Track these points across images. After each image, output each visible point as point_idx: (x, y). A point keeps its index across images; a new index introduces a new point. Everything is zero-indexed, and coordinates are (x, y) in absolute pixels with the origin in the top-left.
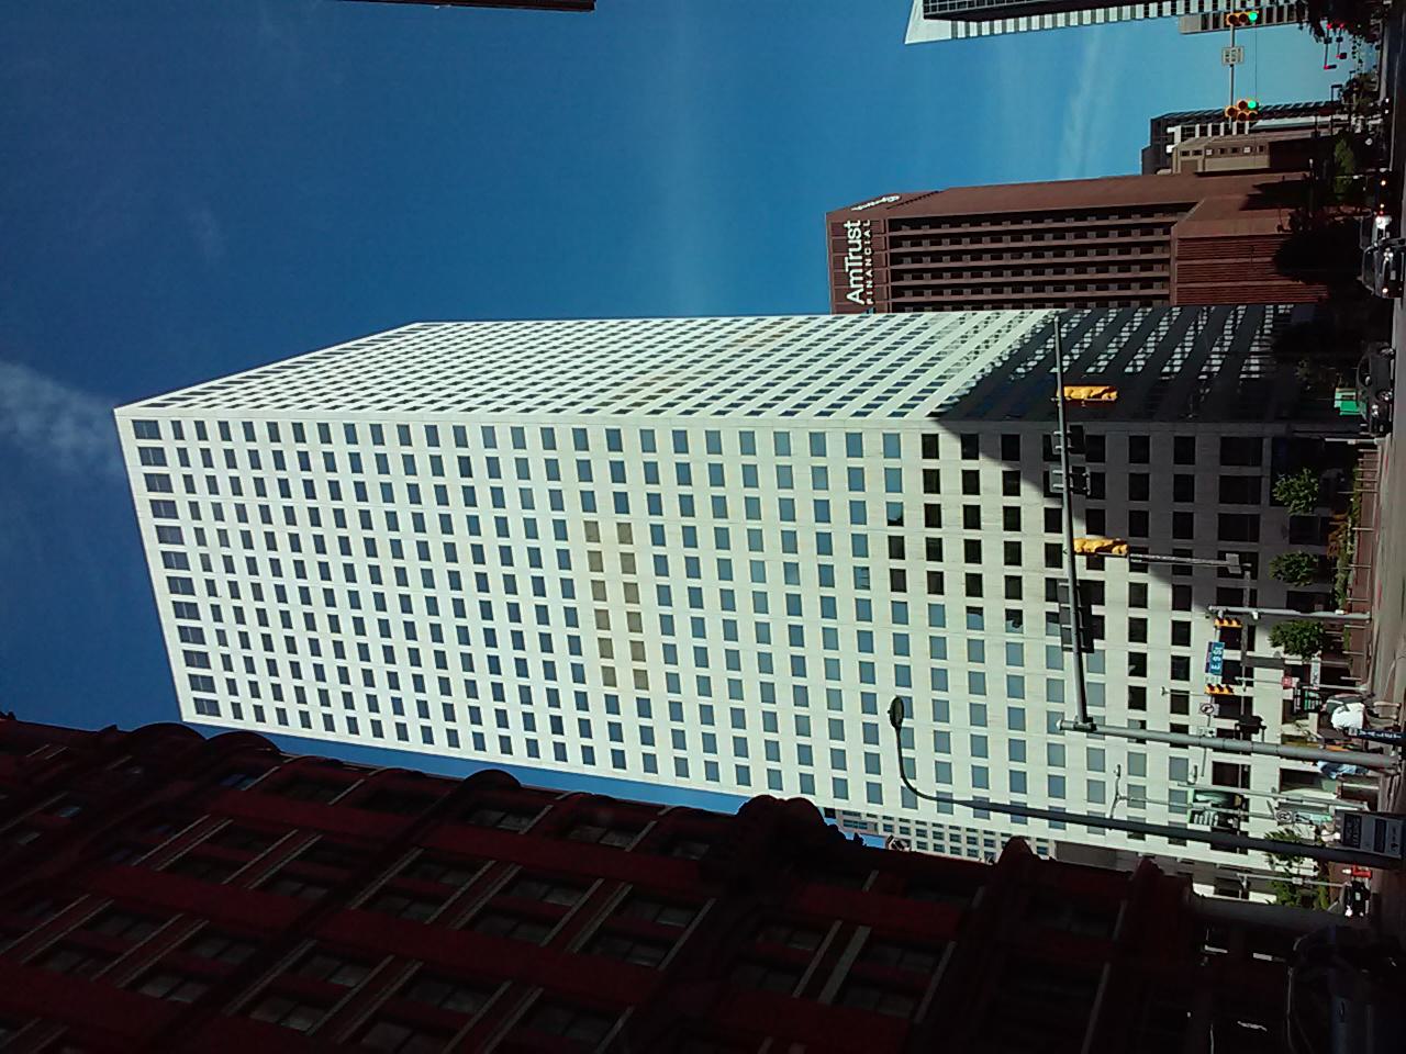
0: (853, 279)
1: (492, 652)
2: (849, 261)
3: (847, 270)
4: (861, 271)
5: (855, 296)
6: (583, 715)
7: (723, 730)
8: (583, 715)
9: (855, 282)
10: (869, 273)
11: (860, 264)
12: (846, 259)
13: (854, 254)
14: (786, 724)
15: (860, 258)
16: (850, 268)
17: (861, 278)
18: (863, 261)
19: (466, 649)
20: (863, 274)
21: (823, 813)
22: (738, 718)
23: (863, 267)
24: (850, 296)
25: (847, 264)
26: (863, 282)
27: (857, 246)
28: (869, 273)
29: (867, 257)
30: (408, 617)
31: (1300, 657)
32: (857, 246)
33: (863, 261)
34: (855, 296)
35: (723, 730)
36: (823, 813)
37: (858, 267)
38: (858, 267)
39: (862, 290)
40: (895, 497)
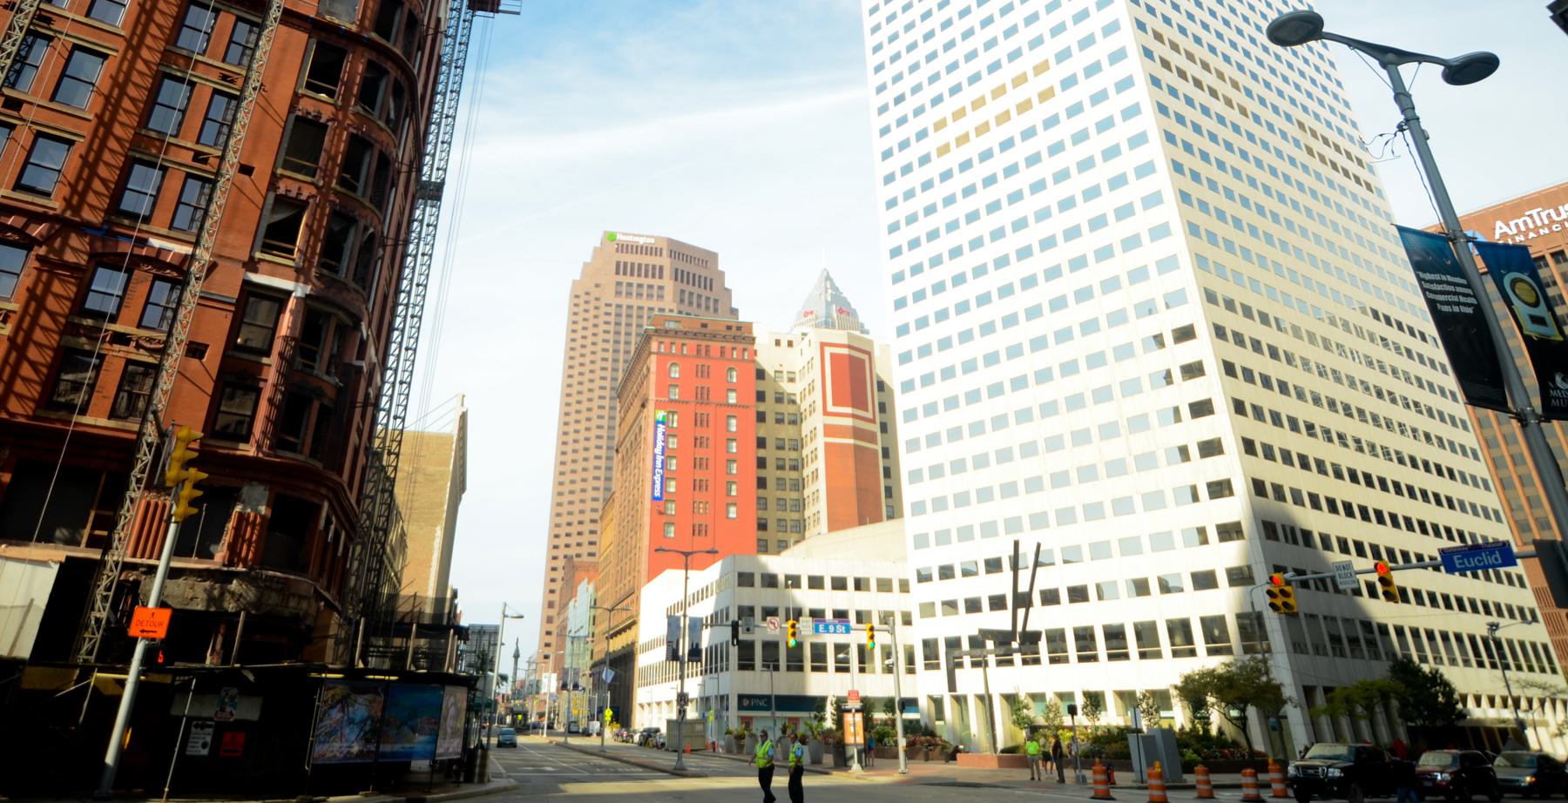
0: (1520, 221)
1: (1118, 119)
2: (1539, 213)
3: (1527, 213)
4: (1531, 226)
5: (1501, 228)
6: (1050, 181)
7: (1108, 202)
8: (1050, 181)
9: (1517, 225)
10: (1531, 235)
11: (1539, 224)
12: (1540, 209)
13: (1549, 216)
14: (1108, 269)
15: (1546, 222)
16: (1531, 216)
17: (1523, 229)
18: (1543, 226)
19: (1093, 131)
20: (1528, 229)
21: (1442, 568)
22: (1124, 212)
23: (1536, 228)
24: (1499, 224)
25: (1534, 212)
26: (1519, 232)
27: (1559, 214)
28: (1531, 235)
29: (1550, 229)
30: (1093, 131)
31: (860, 740)
32: (1559, 214)
33: (1543, 226)
34: (1501, 228)
35: (1108, 202)
36: (1442, 568)
37: (1534, 222)
38: (1534, 222)
39: (1510, 233)
40: (1131, 313)
